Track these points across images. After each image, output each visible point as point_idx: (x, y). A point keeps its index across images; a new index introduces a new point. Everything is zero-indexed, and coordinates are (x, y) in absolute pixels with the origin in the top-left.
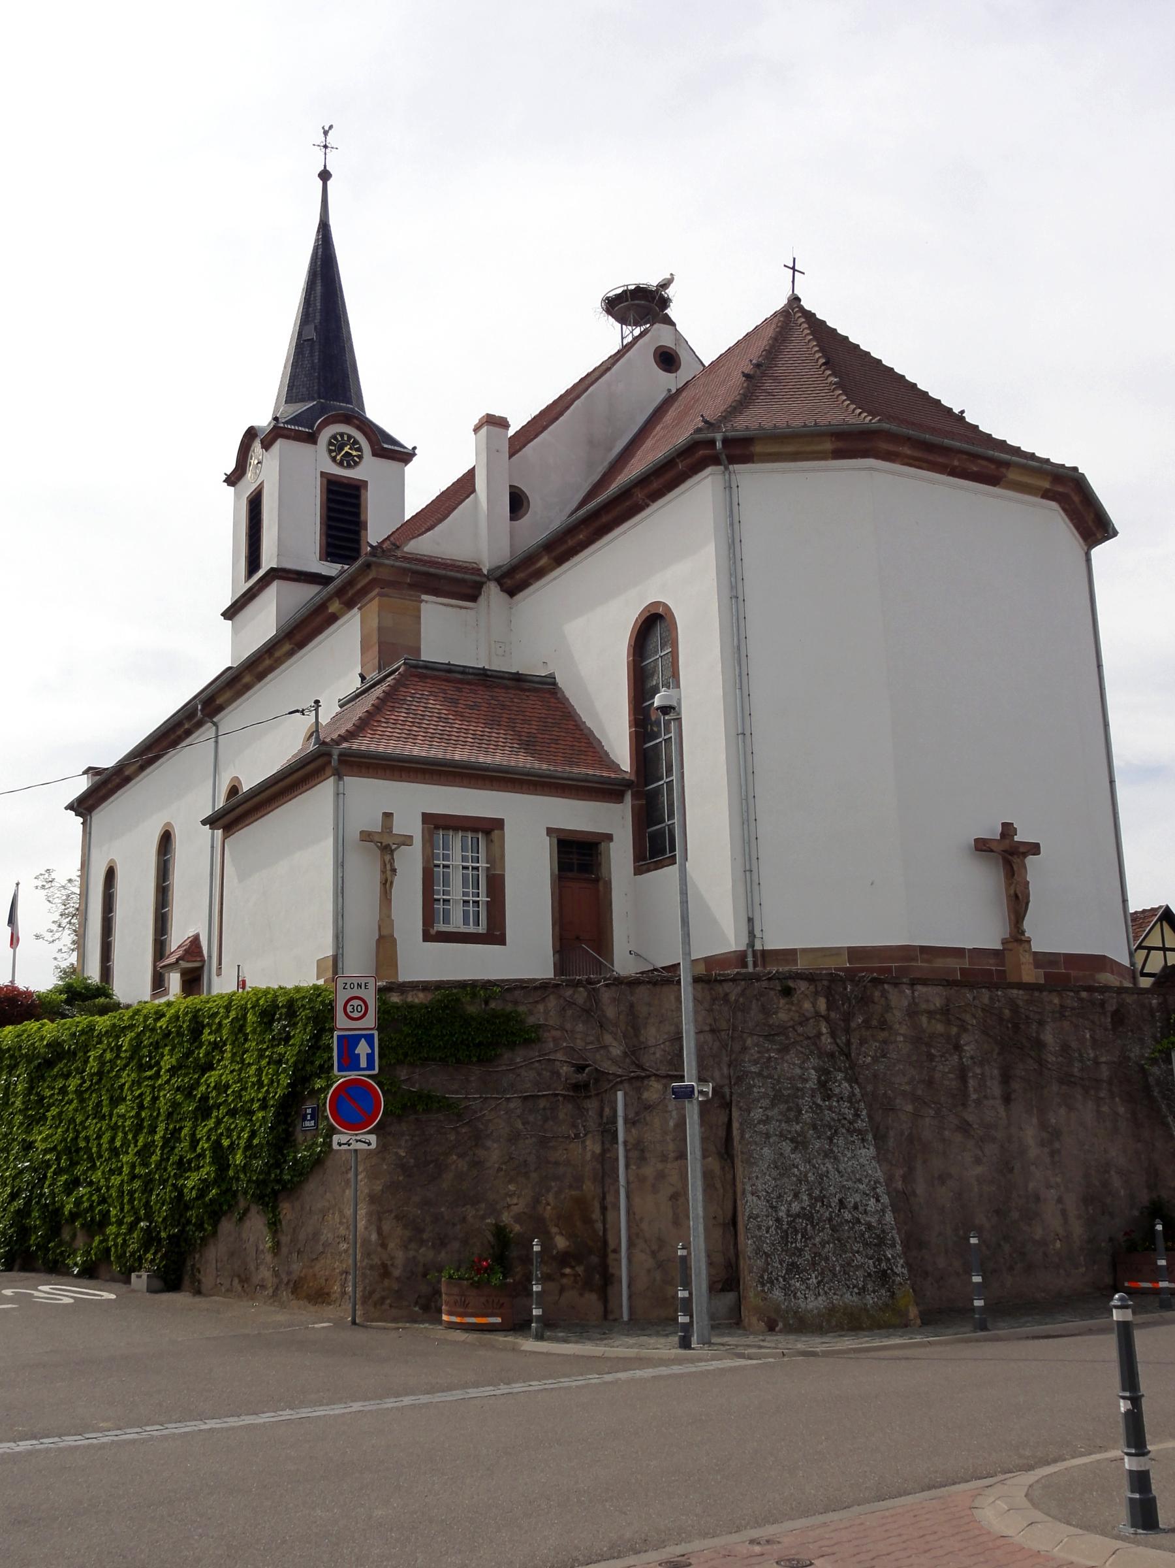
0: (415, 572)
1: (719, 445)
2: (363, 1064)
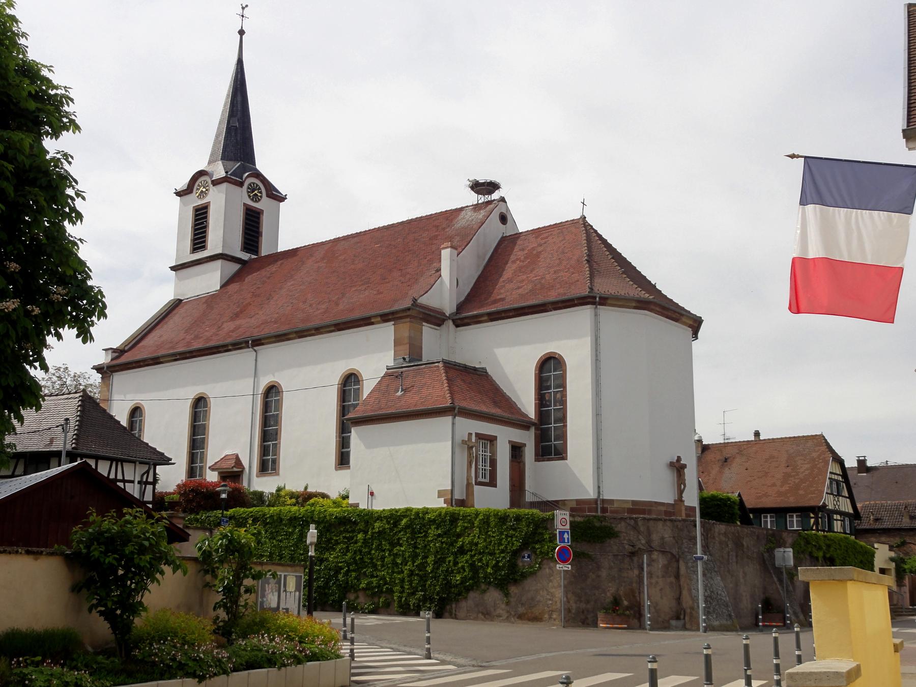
0: (425, 314)
1: (597, 299)
2: (566, 541)
